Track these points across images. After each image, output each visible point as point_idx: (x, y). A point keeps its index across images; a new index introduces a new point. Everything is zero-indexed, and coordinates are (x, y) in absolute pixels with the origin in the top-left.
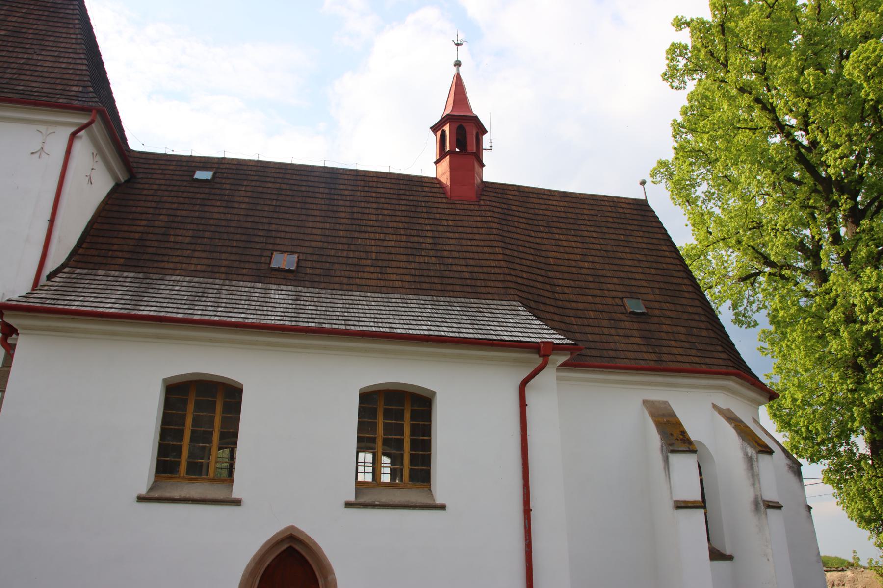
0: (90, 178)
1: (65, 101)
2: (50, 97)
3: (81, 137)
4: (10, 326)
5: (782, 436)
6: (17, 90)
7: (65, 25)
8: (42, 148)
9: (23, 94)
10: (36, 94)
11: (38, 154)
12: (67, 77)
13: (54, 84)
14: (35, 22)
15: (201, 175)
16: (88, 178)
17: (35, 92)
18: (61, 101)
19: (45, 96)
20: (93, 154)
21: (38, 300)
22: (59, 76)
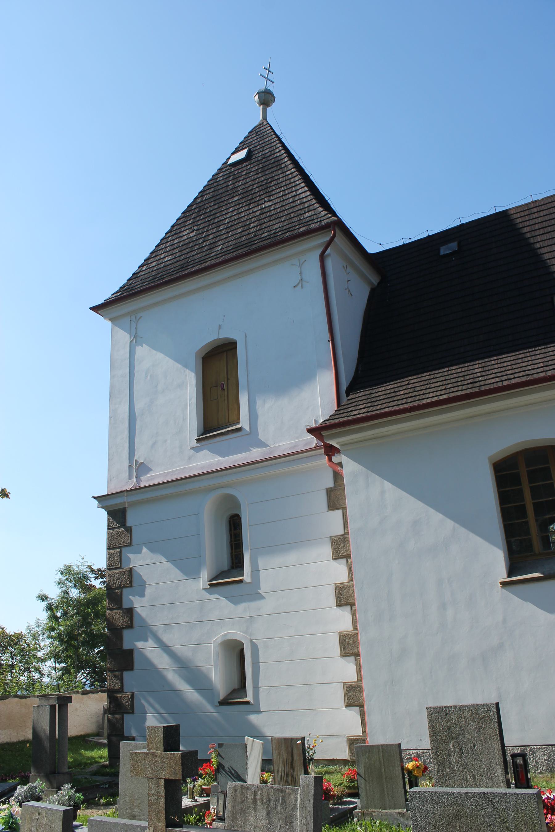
0: (349, 290)
1: (304, 228)
2: (291, 231)
3: (329, 255)
4: (332, 446)
5: (57, 580)
6: (264, 237)
7: (279, 167)
8: (301, 279)
9: (270, 238)
10: (280, 233)
11: (300, 285)
12: (298, 208)
13: (290, 219)
14: (255, 177)
15: (444, 251)
16: (347, 290)
17: (278, 232)
18: (301, 230)
19: (287, 232)
20: (344, 267)
21: (506, 359)
22: (291, 211)
